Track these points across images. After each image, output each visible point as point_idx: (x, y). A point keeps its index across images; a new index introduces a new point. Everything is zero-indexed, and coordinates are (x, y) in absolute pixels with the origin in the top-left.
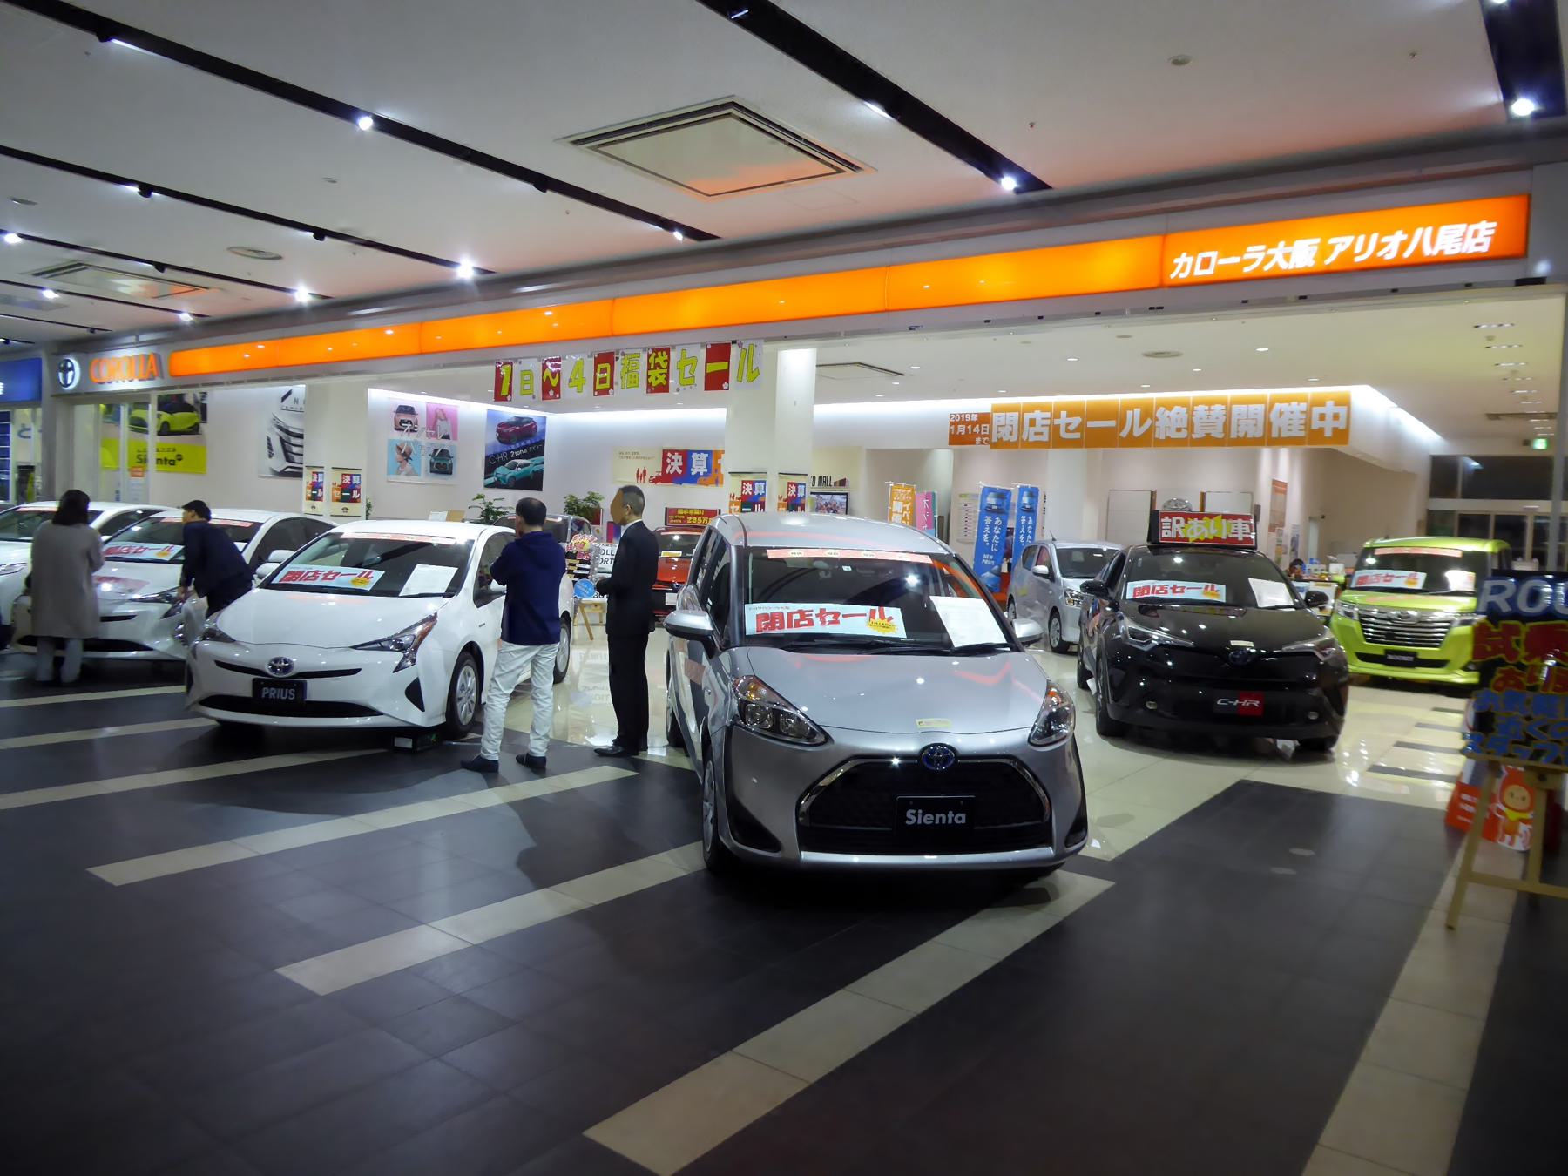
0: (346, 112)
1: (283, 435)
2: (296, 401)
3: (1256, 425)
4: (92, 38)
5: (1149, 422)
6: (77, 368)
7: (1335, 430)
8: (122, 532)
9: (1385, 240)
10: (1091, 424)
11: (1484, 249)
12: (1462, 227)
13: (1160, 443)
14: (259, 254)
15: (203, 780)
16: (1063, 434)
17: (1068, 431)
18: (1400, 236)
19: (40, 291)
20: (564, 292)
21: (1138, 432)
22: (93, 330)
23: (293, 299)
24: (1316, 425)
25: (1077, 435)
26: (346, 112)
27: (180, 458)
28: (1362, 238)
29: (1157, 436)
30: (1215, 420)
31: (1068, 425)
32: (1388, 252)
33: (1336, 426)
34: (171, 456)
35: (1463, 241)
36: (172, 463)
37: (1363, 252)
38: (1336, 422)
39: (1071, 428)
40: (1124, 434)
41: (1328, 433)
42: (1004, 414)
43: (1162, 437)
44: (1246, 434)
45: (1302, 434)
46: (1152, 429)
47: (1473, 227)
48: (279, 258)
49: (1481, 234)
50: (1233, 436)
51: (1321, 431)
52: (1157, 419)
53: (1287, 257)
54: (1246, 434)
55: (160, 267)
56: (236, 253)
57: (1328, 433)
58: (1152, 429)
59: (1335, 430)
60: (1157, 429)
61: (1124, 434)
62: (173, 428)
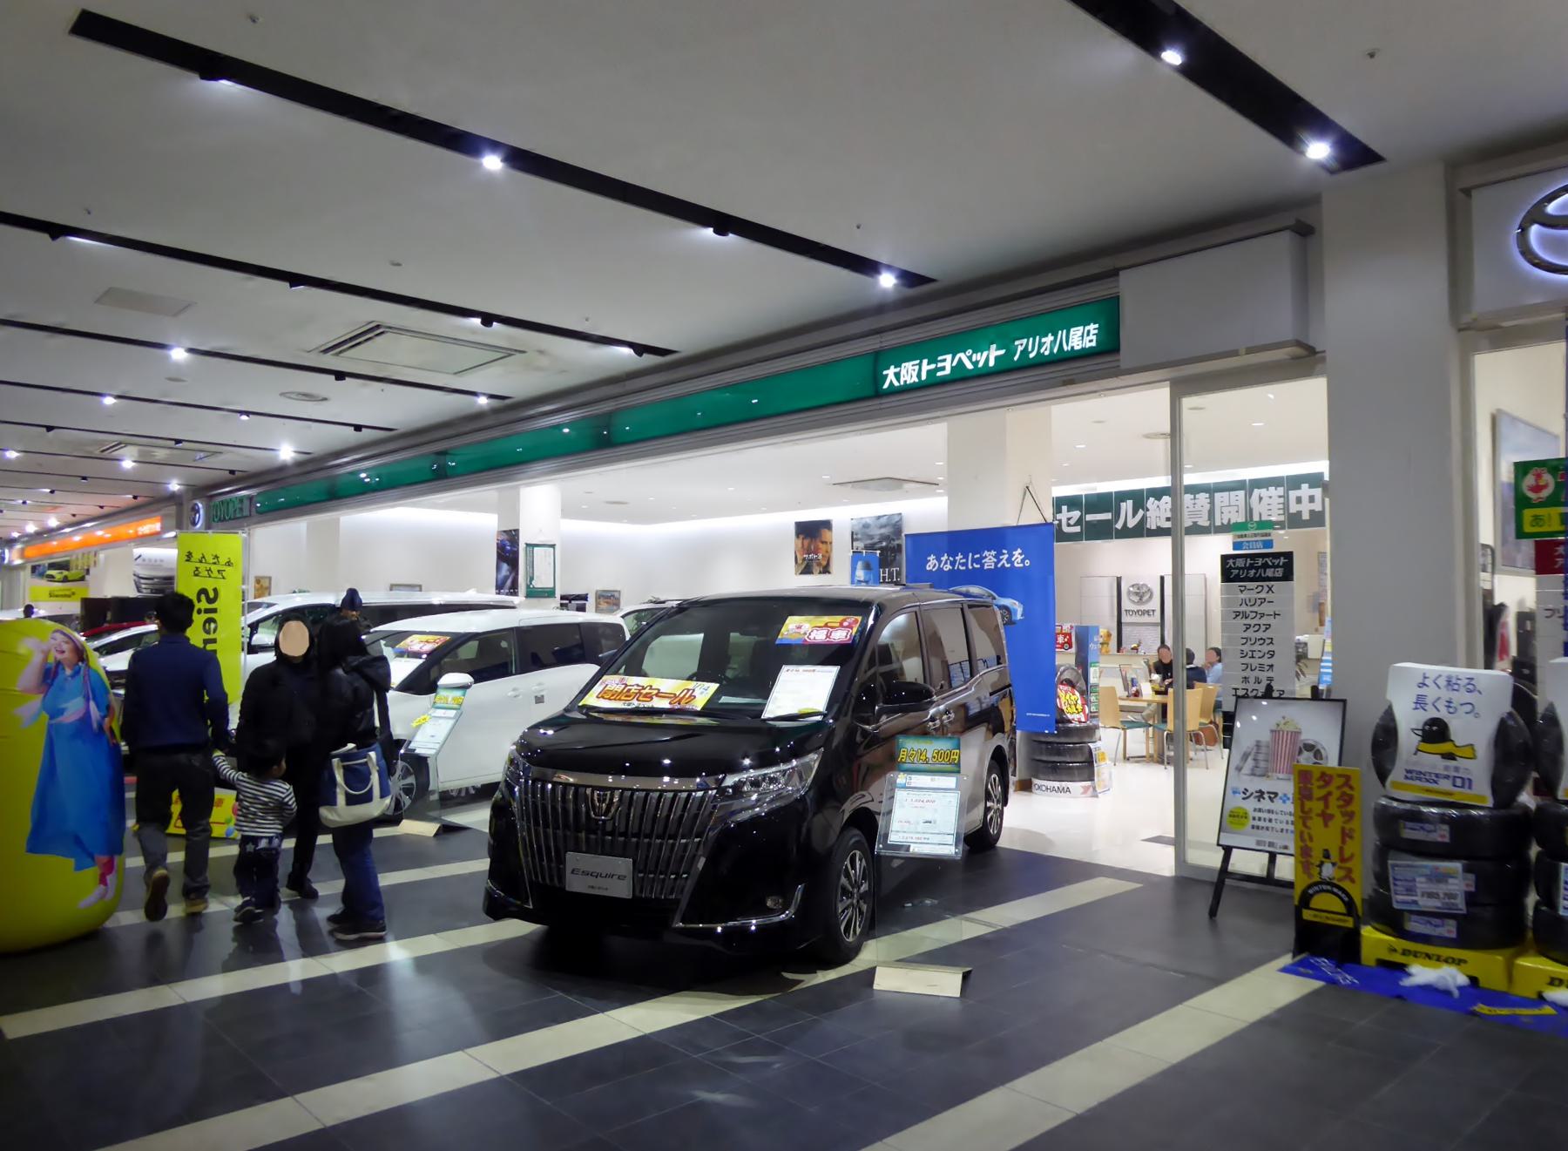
0: (463, 142)
1: (135, 578)
2: (144, 560)
3: (1237, 512)
4: (46, 237)
5: (1141, 512)
6: (202, 512)
7: (1312, 512)
8: (1070, 744)
9: (1043, 340)
10: (1089, 517)
11: (1094, 344)
12: (1081, 328)
13: (69, 581)
14: (308, 397)
15: (1032, 1069)
16: (1066, 529)
17: (1069, 525)
18: (1050, 338)
19: (116, 462)
20: (115, 518)
21: (1132, 523)
22: (232, 472)
23: (277, 456)
24: (1294, 508)
25: (1077, 529)
26: (463, 142)
27: (74, 594)
28: (1031, 339)
29: (1148, 526)
30: (1201, 509)
31: (1069, 519)
32: (1046, 350)
33: (1312, 508)
34: (68, 593)
35: (1082, 340)
36: (69, 596)
37: (1033, 350)
38: (1312, 504)
39: (1072, 522)
40: (1119, 526)
41: (1306, 516)
42: (1227, 493)
43: (1154, 527)
44: (1229, 520)
45: (1282, 518)
46: (1143, 520)
47: (1087, 328)
48: (325, 399)
49: (1092, 332)
50: (1218, 523)
51: (1299, 513)
52: (1148, 510)
53: (897, 375)
54: (1229, 520)
55: (178, 441)
56: (290, 398)
57: (1306, 516)
58: (1143, 520)
59: (1312, 512)
60: (1149, 519)
61: (1119, 526)
62: (70, 579)
